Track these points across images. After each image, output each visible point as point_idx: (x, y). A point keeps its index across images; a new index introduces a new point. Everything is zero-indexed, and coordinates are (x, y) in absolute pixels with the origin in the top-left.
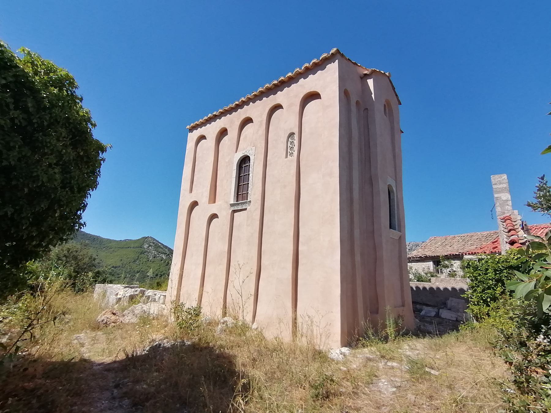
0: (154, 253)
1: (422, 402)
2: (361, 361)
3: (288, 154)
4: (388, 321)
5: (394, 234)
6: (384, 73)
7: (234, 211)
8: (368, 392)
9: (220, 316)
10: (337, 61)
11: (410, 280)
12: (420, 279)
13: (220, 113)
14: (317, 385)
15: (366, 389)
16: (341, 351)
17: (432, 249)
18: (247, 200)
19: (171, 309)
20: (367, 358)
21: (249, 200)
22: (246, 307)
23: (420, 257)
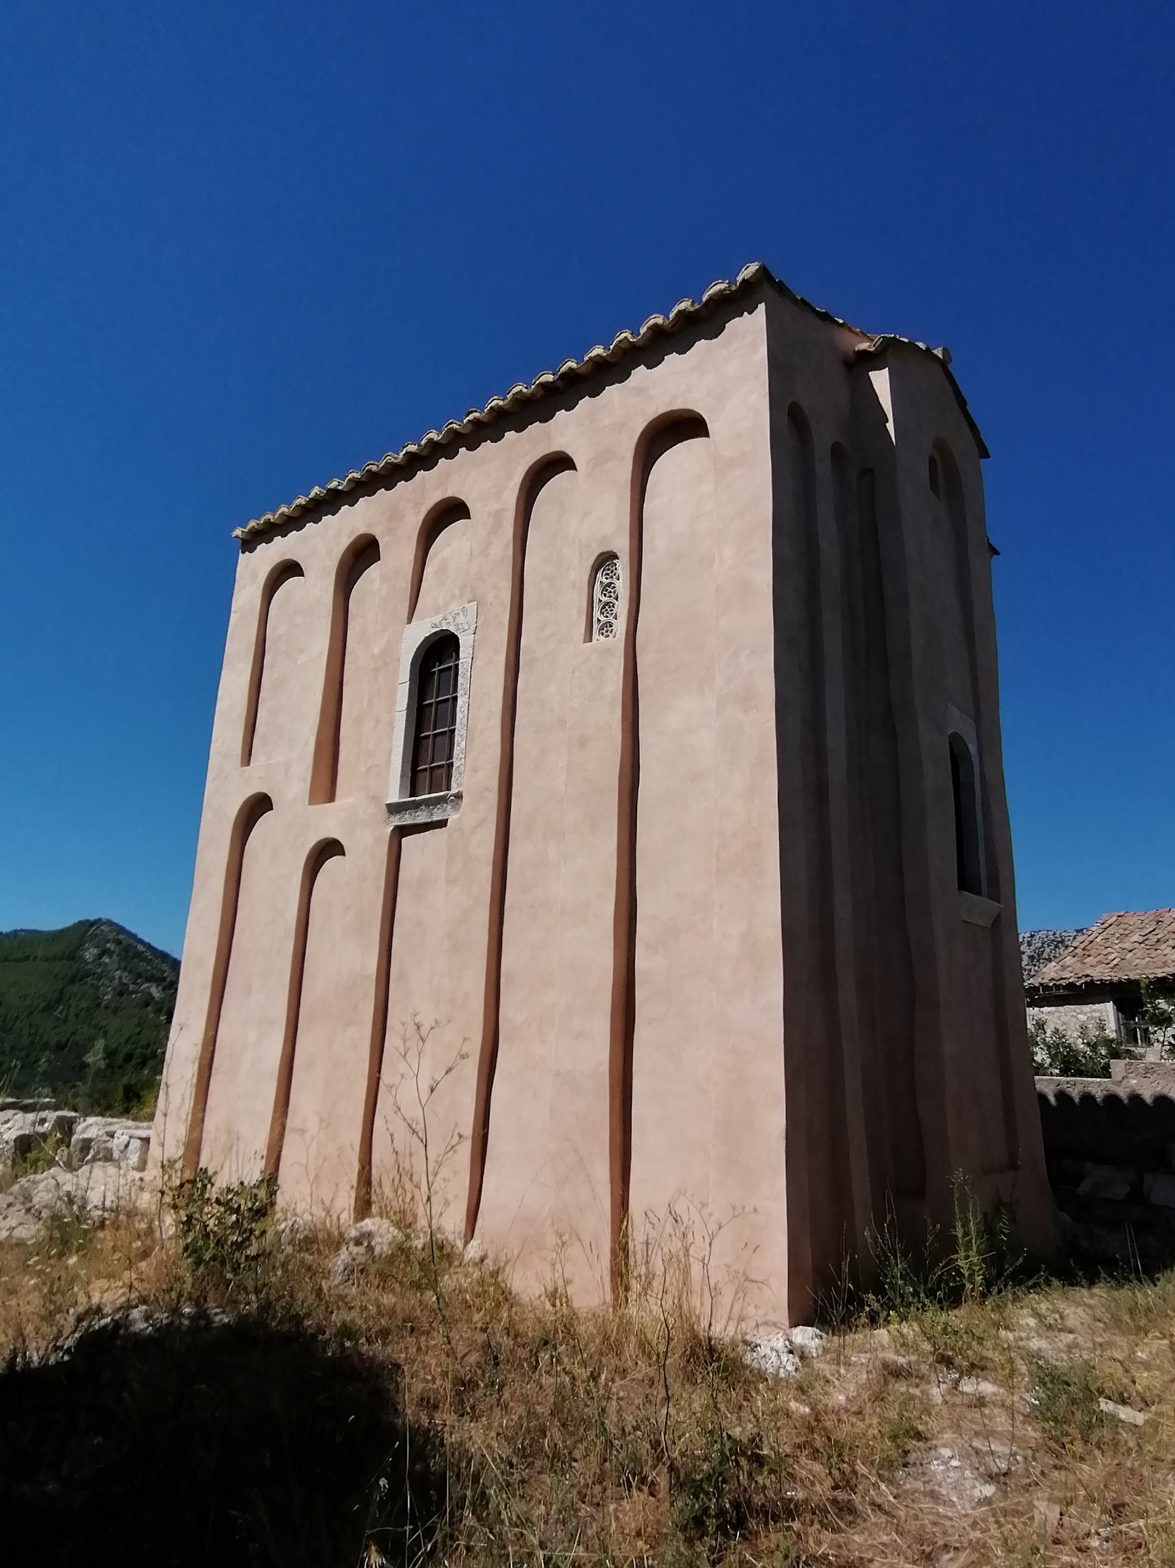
0: (120, 978)
1: (1085, 1526)
2: (865, 1376)
3: (596, 627)
4: (959, 1224)
5: (977, 907)
6: (928, 349)
7: (402, 832)
8: (891, 1498)
9: (347, 1217)
10: (762, 307)
11: (1040, 1069)
12: (1070, 1063)
13: (352, 485)
14: (698, 1477)
15: (883, 1487)
16: (791, 1342)
17: (1111, 957)
18: (449, 789)
19: (163, 1193)
20: (885, 1365)
21: (454, 791)
22: (445, 1180)
23: (1071, 986)
